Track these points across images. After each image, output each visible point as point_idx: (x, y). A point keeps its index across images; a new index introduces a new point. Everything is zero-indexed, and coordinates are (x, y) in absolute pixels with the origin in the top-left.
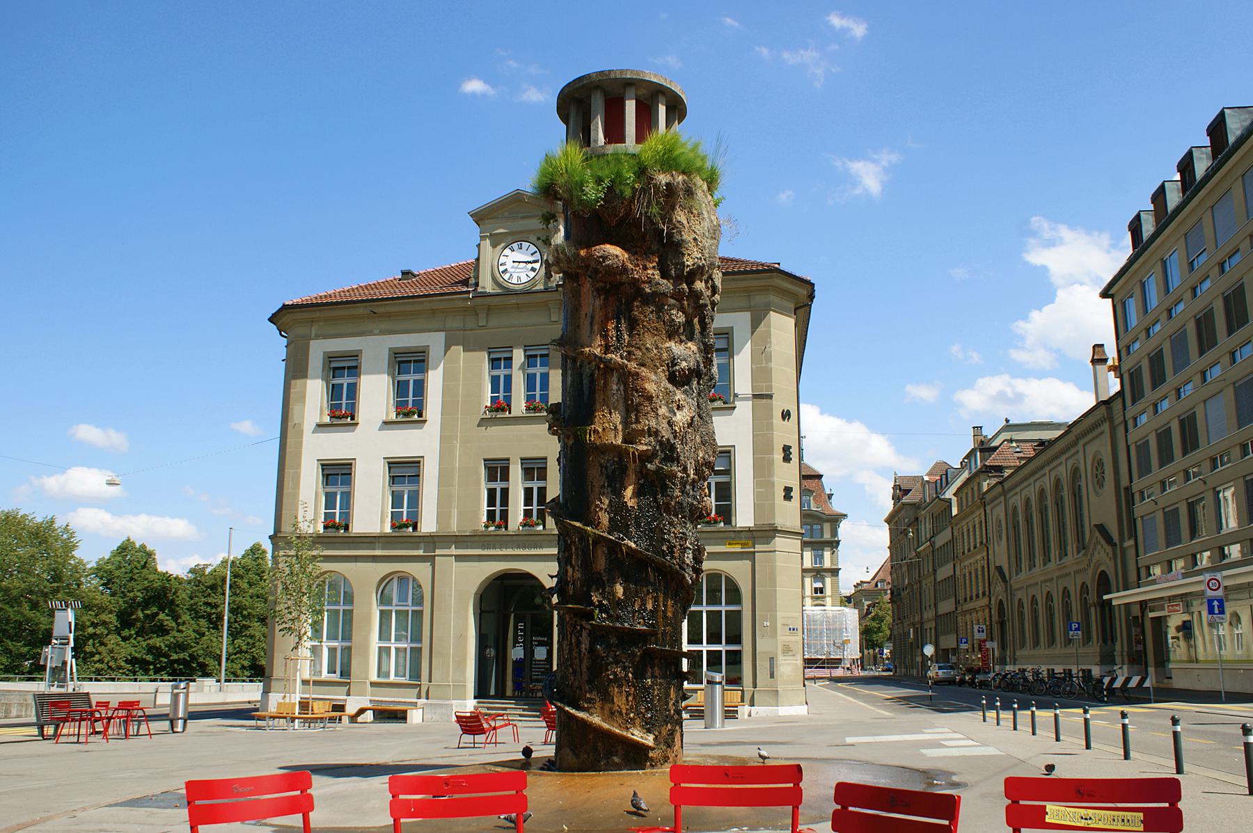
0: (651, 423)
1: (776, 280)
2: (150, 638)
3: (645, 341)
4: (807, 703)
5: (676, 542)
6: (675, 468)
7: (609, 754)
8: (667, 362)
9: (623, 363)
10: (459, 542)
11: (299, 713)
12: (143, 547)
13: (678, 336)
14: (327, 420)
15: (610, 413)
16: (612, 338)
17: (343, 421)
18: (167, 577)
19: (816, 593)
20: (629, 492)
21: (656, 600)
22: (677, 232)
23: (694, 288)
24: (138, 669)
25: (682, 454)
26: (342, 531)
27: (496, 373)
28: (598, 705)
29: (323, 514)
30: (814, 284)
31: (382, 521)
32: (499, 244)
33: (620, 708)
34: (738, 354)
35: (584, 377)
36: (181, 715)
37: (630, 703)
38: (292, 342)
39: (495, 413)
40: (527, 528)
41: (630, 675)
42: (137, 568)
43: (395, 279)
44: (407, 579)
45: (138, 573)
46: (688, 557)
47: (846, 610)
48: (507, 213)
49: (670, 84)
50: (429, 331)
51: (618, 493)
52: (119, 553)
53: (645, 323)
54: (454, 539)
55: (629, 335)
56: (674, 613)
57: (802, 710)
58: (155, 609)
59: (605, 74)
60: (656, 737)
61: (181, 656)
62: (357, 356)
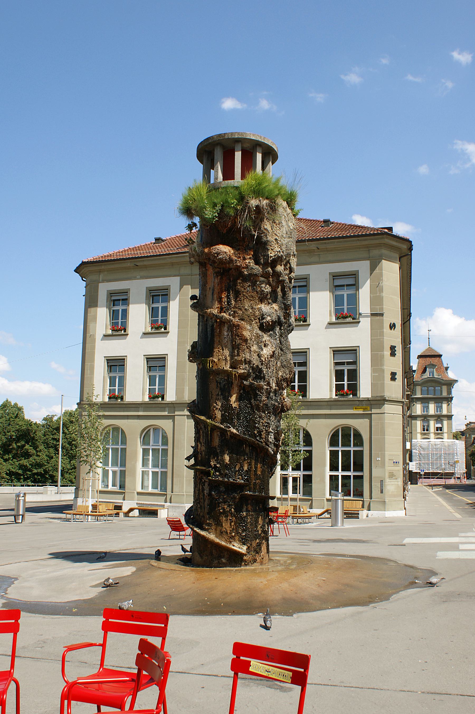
0: (246, 356)
1: (386, 240)
2: (21, 460)
4: (405, 509)
5: (263, 428)
6: (262, 383)
7: (220, 557)
8: (258, 317)
9: (230, 319)
11: (91, 511)
12: (16, 404)
13: (267, 300)
14: (110, 332)
15: (223, 350)
16: (224, 303)
17: (119, 333)
18: (30, 423)
19: (437, 430)
20: (233, 398)
21: (250, 464)
22: (264, 235)
23: (276, 270)
24: (14, 479)
25: (266, 375)
26: (120, 400)
28: (213, 527)
29: (108, 390)
30: (411, 241)
31: (143, 394)
33: (226, 529)
34: (361, 288)
35: (208, 327)
36: (21, 513)
37: (232, 527)
38: (88, 285)
41: (233, 510)
42: (12, 418)
43: (151, 243)
44: (159, 429)
45: (13, 421)
46: (271, 438)
47: (457, 441)
49: (264, 140)
50: (170, 276)
51: (227, 399)
52: (2, 409)
53: (244, 294)
55: (235, 301)
56: (262, 472)
57: (401, 513)
58: (23, 443)
59: (222, 136)
60: (249, 547)
61: (39, 470)
62: (127, 292)
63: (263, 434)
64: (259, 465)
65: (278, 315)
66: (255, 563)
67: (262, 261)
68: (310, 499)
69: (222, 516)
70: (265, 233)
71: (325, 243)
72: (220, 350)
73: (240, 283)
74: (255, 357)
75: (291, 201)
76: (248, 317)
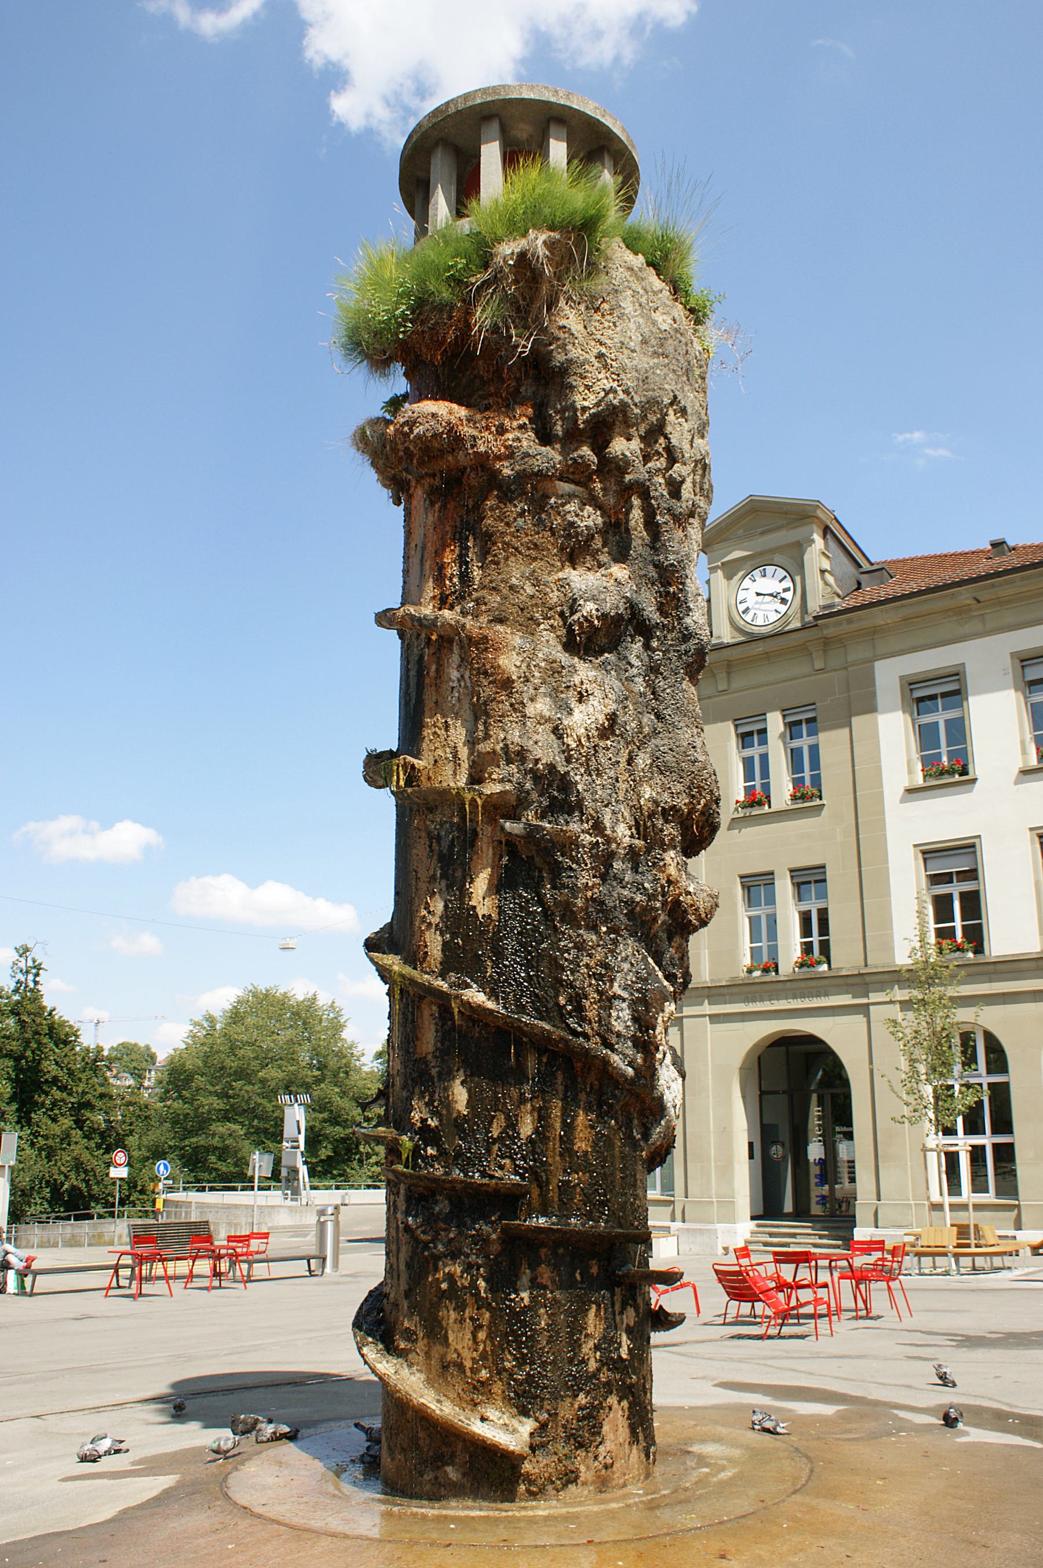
3: (508, 573)
5: (590, 985)
6: (575, 827)
7: (439, 1461)
10: (713, 996)
16: (451, 580)
20: (480, 885)
21: (542, 1117)
22: (558, 347)
27: (748, 752)
28: (421, 1345)
32: (735, 575)
33: (459, 1355)
37: (481, 1347)
39: (749, 809)
40: (805, 969)
41: (482, 1284)
46: (618, 1017)
48: (742, 531)
53: (507, 539)
54: (706, 992)
60: (543, 1426)
63: (587, 1004)
64: (581, 1118)
65: (627, 597)
66: (572, 1487)
67: (559, 428)
68: (1015, 1205)
69: (447, 1308)
70: (559, 339)
71: (993, 586)
72: (440, 729)
73: (492, 509)
74: (544, 734)
75: (665, 257)
76: (522, 610)
